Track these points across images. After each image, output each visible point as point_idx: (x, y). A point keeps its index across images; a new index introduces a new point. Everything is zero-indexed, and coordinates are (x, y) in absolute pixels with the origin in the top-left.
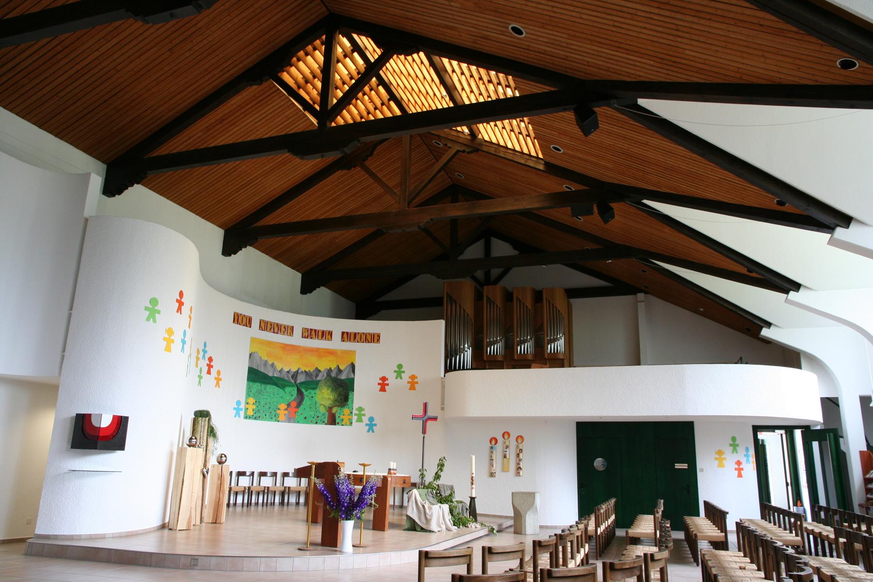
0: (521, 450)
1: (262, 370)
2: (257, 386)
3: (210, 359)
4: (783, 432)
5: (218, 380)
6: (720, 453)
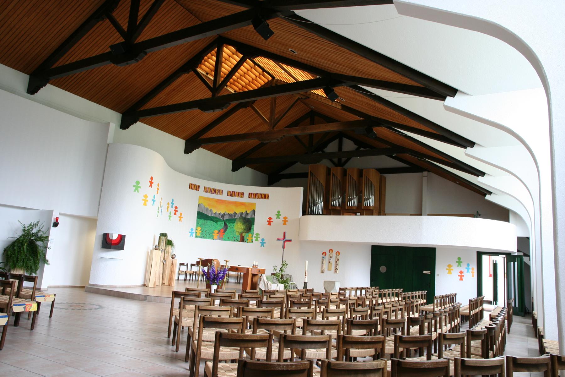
0: (338, 260)
1: (205, 212)
2: (202, 221)
3: (176, 207)
4: (505, 256)
5: (181, 218)
6: (450, 266)
